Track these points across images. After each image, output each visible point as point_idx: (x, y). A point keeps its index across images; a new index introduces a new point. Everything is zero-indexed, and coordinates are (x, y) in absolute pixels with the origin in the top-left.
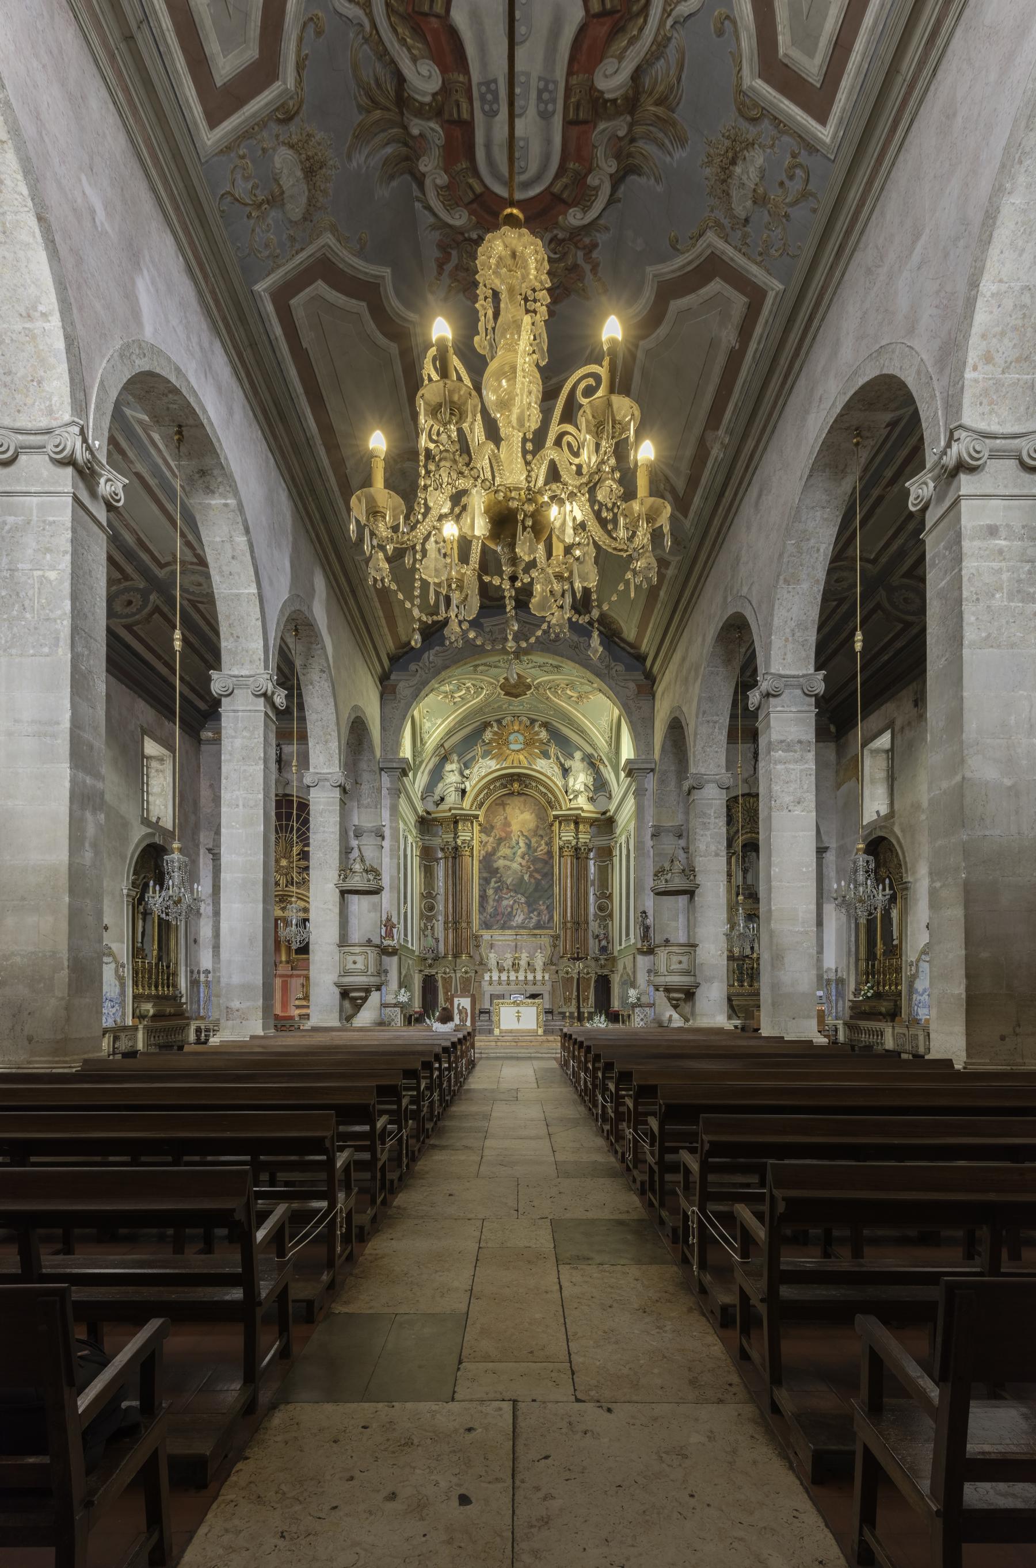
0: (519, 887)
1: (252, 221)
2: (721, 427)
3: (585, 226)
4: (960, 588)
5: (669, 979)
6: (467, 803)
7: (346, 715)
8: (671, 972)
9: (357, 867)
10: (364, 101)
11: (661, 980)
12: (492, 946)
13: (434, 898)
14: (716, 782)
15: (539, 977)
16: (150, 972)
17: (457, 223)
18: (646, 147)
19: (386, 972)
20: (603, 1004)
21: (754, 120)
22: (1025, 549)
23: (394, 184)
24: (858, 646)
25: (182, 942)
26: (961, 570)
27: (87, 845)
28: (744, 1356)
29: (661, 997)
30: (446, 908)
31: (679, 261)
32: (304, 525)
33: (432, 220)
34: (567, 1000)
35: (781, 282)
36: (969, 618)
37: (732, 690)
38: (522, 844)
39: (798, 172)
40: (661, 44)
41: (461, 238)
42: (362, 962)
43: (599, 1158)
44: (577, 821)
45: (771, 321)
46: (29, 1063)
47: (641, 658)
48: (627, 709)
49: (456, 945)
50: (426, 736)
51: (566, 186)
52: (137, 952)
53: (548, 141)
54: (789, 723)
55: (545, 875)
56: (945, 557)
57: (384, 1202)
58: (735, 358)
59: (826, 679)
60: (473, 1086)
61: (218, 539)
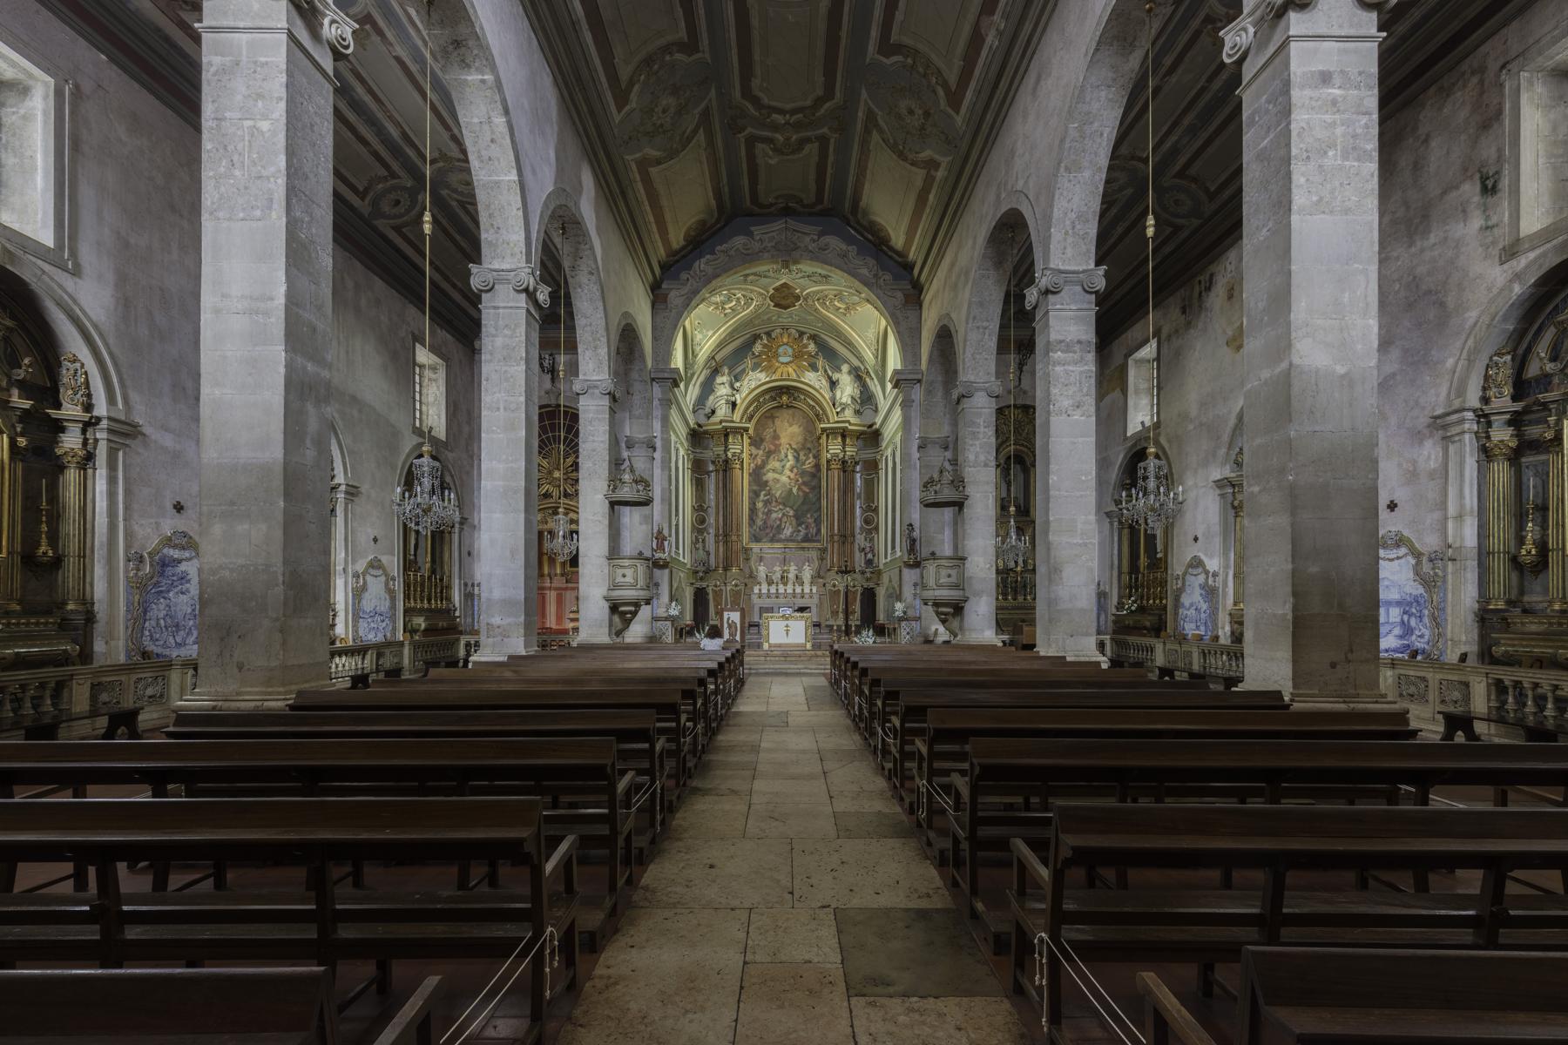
0: (786, 500)
4: (1288, 145)
5: (937, 593)
6: (737, 416)
7: (615, 320)
8: (940, 586)
9: (627, 477)
11: (929, 594)
12: (761, 559)
13: (705, 511)
14: (985, 390)
15: (807, 590)
16: (422, 585)
19: (657, 585)
20: (869, 618)
22: (1362, 99)
24: (1150, 232)
25: (456, 554)
26: (1289, 124)
27: (308, 442)
28: (955, 884)
29: (929, 611)
30: (717, 521)
32: (571, 117)
34: (835, 613)
36: (1298, 179)
37: (1002, 295)
38: (790, 457)
42: (631, 578)
43: (879, 806)
44: (844, 434)
46: (238, 694)
47: (909, 267)
48: (895, 321)
49: (726, 558)
50: (697, 349)
52: (409, 565)
54: (1068, 324)
55: (813, 489)
56: (1267, 111)
57: (629, 882)
59: (1106, 275)
60: (742, 708)
61: (476, 120)
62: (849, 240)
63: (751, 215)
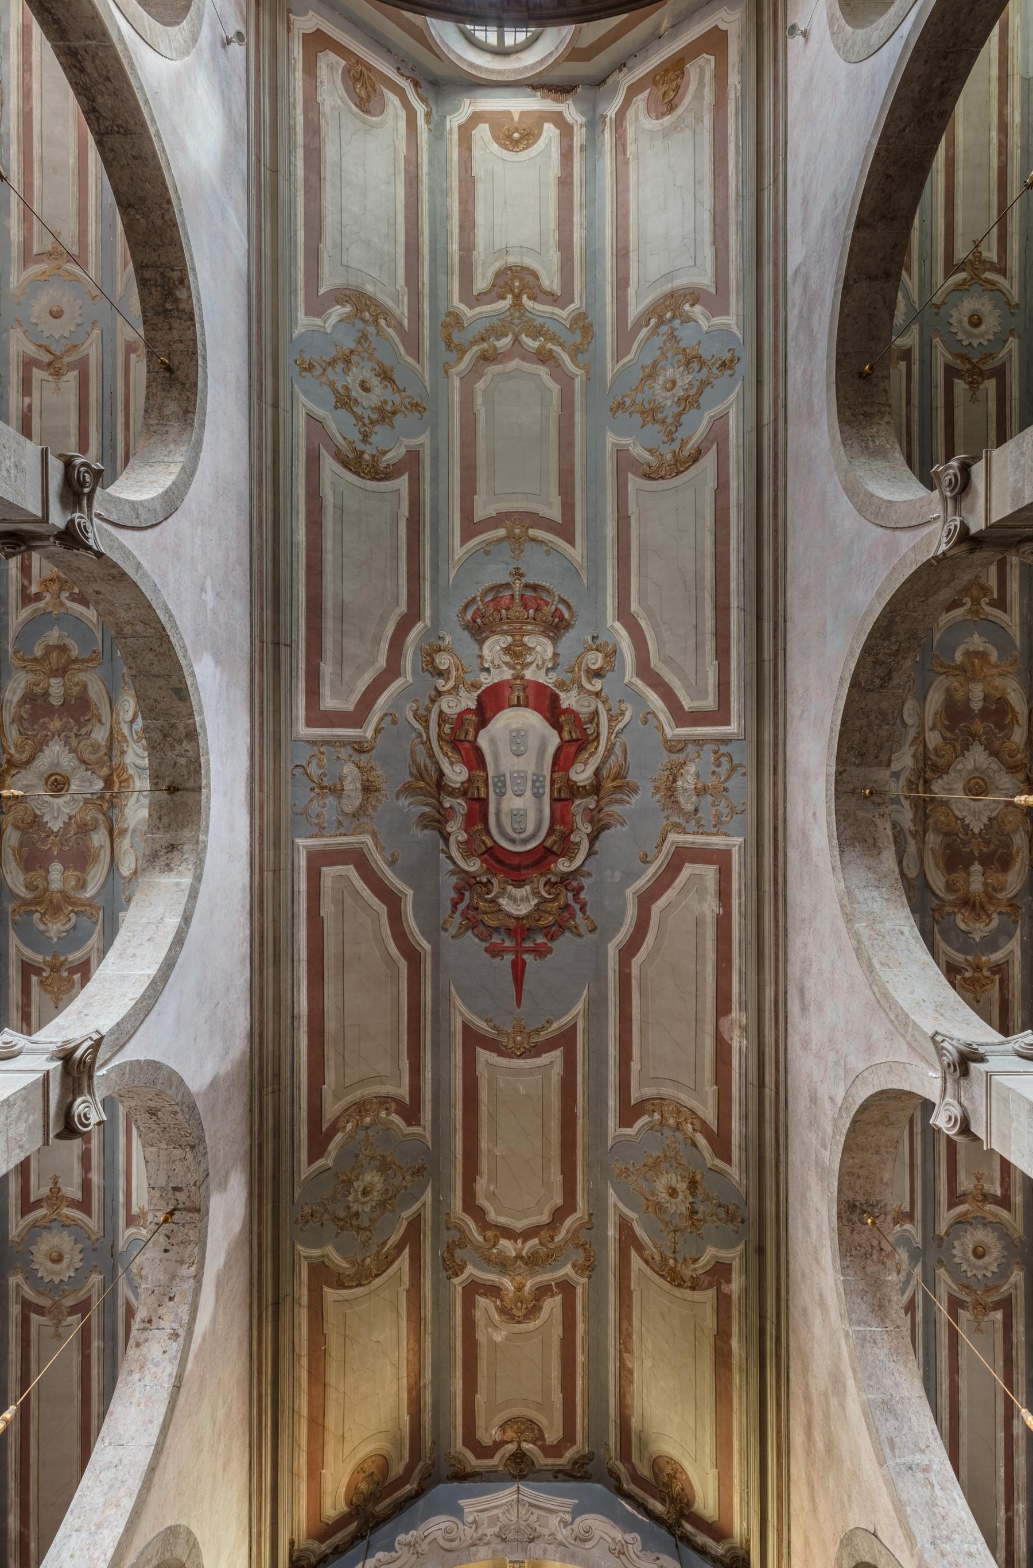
1: (313, 794)
2: (733, 1006)
3: (572, 872)
10: (415, 771)
17: (472, 869)
18: (612, 809)
21: (680, 751)
23: (427, 832)
31: (652, 869)
33: (452, 867)
35: (739, 836)
39: (723, 759)
40: (610, 751)
41: (474, 881)
45: (743, 872)
51: (555, 842)
53: (541, 811)
58: (723, 924)
62: (627, 1524)
63: (461, 1476)
